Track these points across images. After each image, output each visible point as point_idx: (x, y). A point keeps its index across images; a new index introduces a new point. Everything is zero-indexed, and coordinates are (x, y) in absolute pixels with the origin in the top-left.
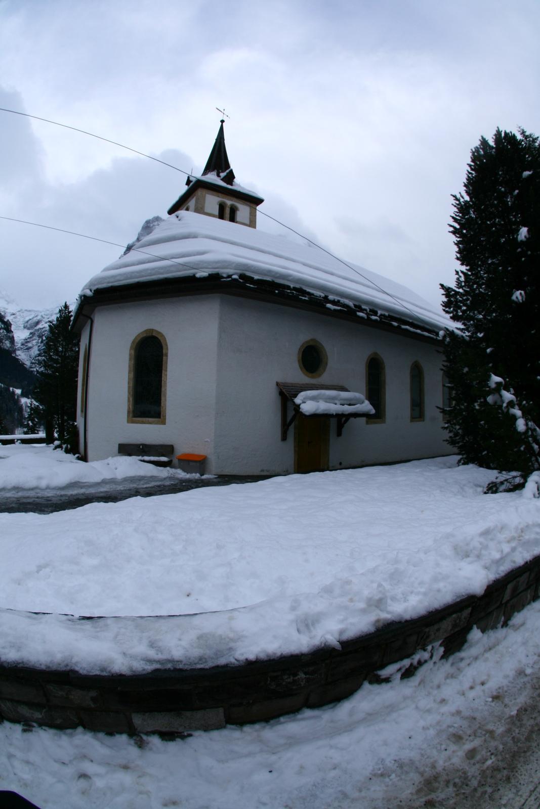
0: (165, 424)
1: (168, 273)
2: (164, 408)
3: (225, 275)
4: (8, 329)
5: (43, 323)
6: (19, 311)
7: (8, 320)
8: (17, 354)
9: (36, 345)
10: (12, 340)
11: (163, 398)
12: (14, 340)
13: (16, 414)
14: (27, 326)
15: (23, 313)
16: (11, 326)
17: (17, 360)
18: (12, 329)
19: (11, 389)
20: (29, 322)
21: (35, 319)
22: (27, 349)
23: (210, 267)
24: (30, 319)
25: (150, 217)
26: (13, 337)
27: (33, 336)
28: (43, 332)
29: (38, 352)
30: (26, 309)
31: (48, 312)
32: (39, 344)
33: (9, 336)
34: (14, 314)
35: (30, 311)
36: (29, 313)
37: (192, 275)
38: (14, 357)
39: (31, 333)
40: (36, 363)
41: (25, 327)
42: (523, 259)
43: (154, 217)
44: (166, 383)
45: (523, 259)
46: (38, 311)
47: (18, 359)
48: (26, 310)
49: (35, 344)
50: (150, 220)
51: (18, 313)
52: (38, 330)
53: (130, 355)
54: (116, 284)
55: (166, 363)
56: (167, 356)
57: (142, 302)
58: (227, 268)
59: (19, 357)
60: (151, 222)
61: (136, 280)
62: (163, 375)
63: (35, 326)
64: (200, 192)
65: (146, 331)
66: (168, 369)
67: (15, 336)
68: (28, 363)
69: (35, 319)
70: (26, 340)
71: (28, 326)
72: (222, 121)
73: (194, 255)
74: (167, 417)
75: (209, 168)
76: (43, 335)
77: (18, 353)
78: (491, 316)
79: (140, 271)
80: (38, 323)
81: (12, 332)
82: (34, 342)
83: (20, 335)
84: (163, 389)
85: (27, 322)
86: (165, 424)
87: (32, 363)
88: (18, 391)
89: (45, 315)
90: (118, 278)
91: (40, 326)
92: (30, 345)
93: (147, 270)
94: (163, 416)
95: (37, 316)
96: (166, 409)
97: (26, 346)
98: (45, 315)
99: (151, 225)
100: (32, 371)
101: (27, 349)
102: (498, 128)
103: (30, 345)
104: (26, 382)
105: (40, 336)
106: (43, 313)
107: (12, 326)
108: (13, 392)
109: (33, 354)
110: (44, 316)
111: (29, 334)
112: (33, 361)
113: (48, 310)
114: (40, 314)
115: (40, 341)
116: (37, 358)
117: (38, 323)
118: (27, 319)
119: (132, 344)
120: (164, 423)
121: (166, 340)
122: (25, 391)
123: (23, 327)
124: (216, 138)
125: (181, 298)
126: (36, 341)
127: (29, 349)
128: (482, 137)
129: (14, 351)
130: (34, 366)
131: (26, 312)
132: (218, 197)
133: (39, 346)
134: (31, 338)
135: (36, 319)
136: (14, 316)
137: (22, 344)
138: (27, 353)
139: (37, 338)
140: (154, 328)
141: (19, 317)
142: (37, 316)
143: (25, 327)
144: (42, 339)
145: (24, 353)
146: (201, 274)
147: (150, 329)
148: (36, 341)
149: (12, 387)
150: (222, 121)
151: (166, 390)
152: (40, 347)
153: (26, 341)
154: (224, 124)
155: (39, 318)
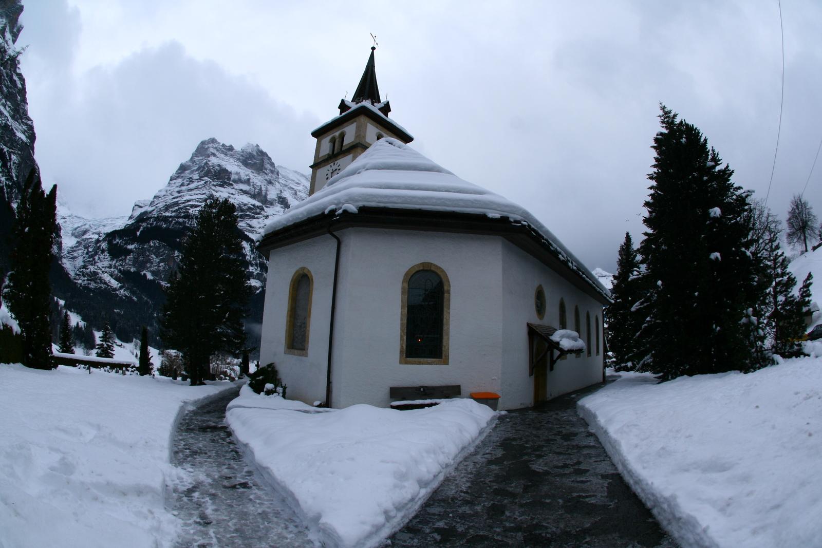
0: (448, 364)
1: (454, 207)
2: (447, 348)
3: (512, 220)
4: (58, 233)
5: (90, 233)
6: (70, 216)
7: (59, 224)
8: (63, 262)
9: (82, 255)
10: (60, 245)
11: (445, 337)
12: (62, 246)
13: (59, 326)
14: (74, 234)
15: (72, 218)
16: (60, 231)
17: (63, 269)
18: (61, 234)
19: (56, 298)
20: (78, 230)
21: (83, 227)
22: (73, 258)
23: (499, 209)
24: (79, 227)
25: (206, 138)
26: (61, 243)
27: (79, 246)
28: (89, 243)
29: (83, 264)
30: (76, 215)
31: (96, 223)
32: (84, 256)
33: (58, 241)
34: (64, 218)
35: (79, 218)
36: (78, 220)
37: (320, 213)
38: (60, 265)
39: (78, 242)
40: (80, 275)
41: (73, 234)
42: (738, 258)
43: (211, 138)
44: (448, 320)
45: (738, 258)
46: (87, 220)
47: (64, 267)
48: (76, 216)
49: (80, 254)
50: (206, 141)
51: (68, 218)
52: (85, 240)
53: (403, 288)
54: (390, 206)
55: (449, 300)
56: (449, 292)
57: (439, 233)
58: (514, 214)
59: (64, 266)
60: (206, 143)
61: (418, 207)
62: (445, 313)
63: (83, 235)
64: (363, 119)
65: (423, 264)
66: (451, 307)
67: (63, 242)
68: (72, 274)
69: (83, 227)
70: (73, 248)
71: (76, 234)
72: (373, 49)
73: (471, 193)
74: (450, 357)
75: (359, 96)
76: (89, 246)
77: (64, 260)
78: (68, 307)
79: (423, 198)
80: (85, 232)
81: (61, 237)
82: (80, 251)
83: (68, 242)
84: (445, 328)
85: (76, 229)
86: (448, 364)
87: (76, 274)
88: (62, 302)
89: (93, 224)
90: (394, 200)
91: (87, 236)
92: (75, 254)
93: (431, 198)
94: (445, 356)
95: (85, 225)
96: (448, 348)
97: (72, 255)
98: (93, 224)
99: (206, 146)
100: (76, 283)
101: (73, 258)
102: (663, 109)
103: (75, 254)
104: (70, 294)
105: (86, 247)
106: (91, 223)
107: (62, 231)
108: (57, 303)
109: (78, 265)
110: (92, 226)
111: (76, 243)
112: (78, 272)
113: (96, 221)
114: (89, 223)
115: (85, 252)
116: (82, 270)
117: (85, 232)
118: (76, 226)
119: (404, 277)
120: (446, 363)
121: (447, 276)
122: (68, 303)
123: (70, 234)
124: (366, 65)
125: (485, 236)
126: (82, 251)
127: (74, 258)
128: (668, 118)
129: (61, 258)
130: (78, 277)
131: (75, 218)
132: (377, 127)
133: (84, 257)
134: (77, 247)
135: (83, 228)
136: (64, 220)
137: (69, 253)
138: (72, 262)
139: (83, 248)
140: (433, 262)
141: (68, 222)
142: (85, 225)
143: (73, 234)
144: (88, 250)
145: (69, 262)
146: (492, 214)
147: (429, 263)
148: (82, 251)
149: (56, 296)
150: (373, 49)
151: (448, 328)
152: (85, 259)
153: (73, 250)
154: (374, 51)
155: (87, 227)
